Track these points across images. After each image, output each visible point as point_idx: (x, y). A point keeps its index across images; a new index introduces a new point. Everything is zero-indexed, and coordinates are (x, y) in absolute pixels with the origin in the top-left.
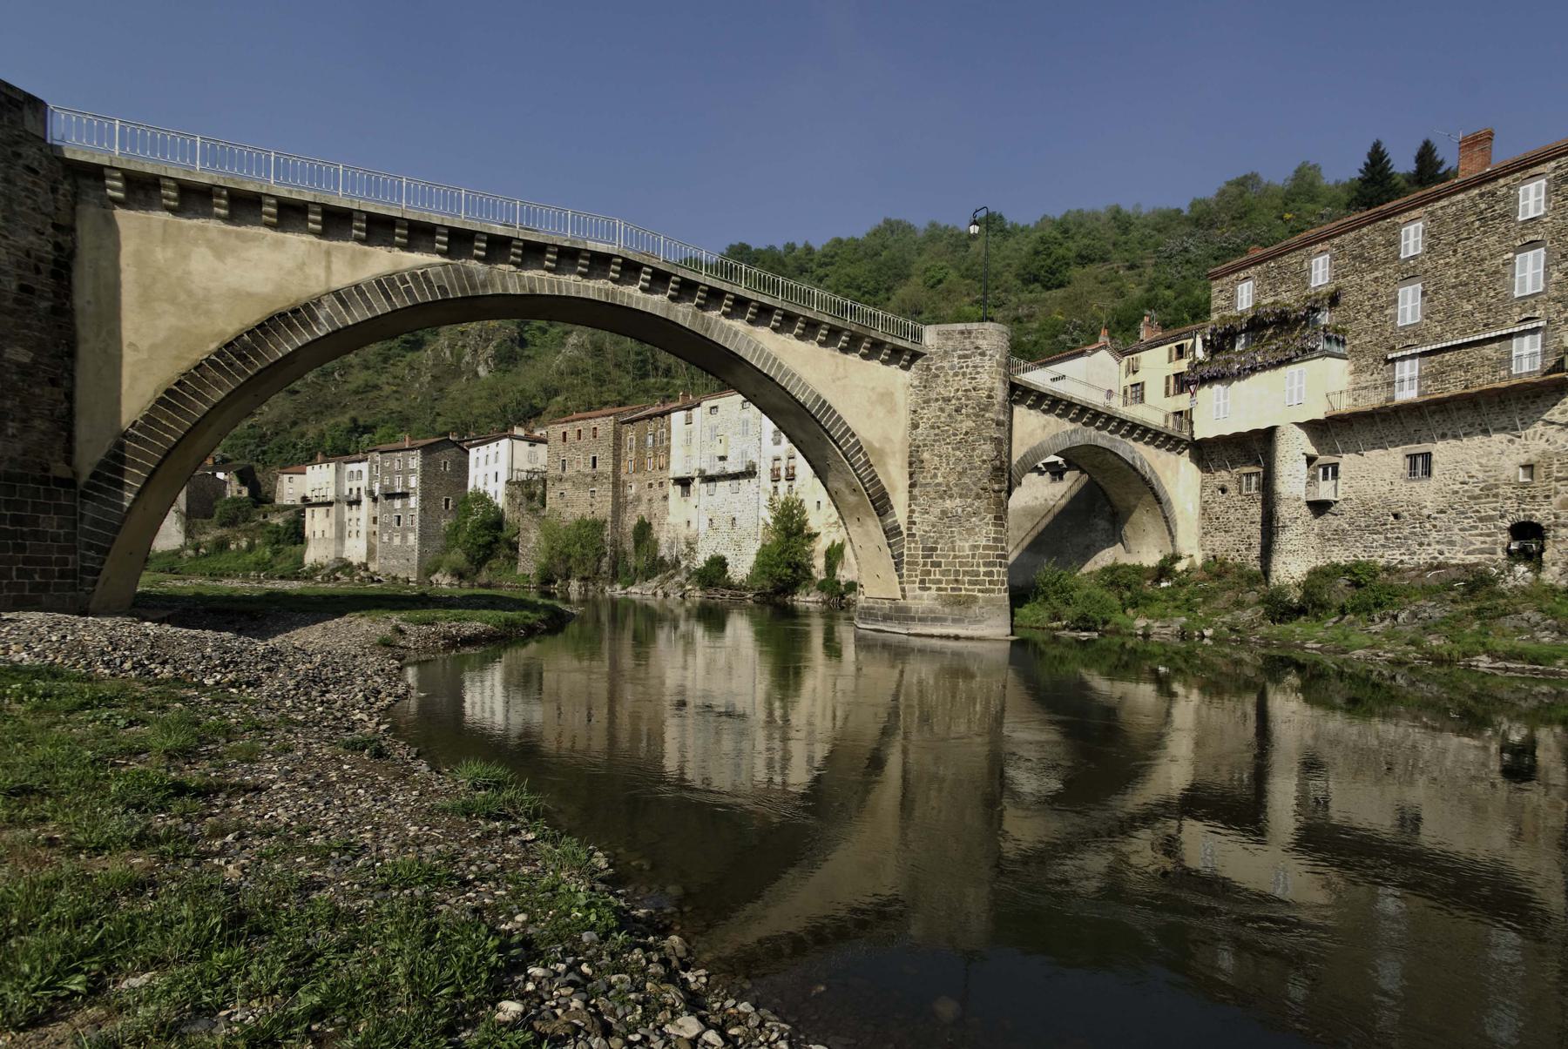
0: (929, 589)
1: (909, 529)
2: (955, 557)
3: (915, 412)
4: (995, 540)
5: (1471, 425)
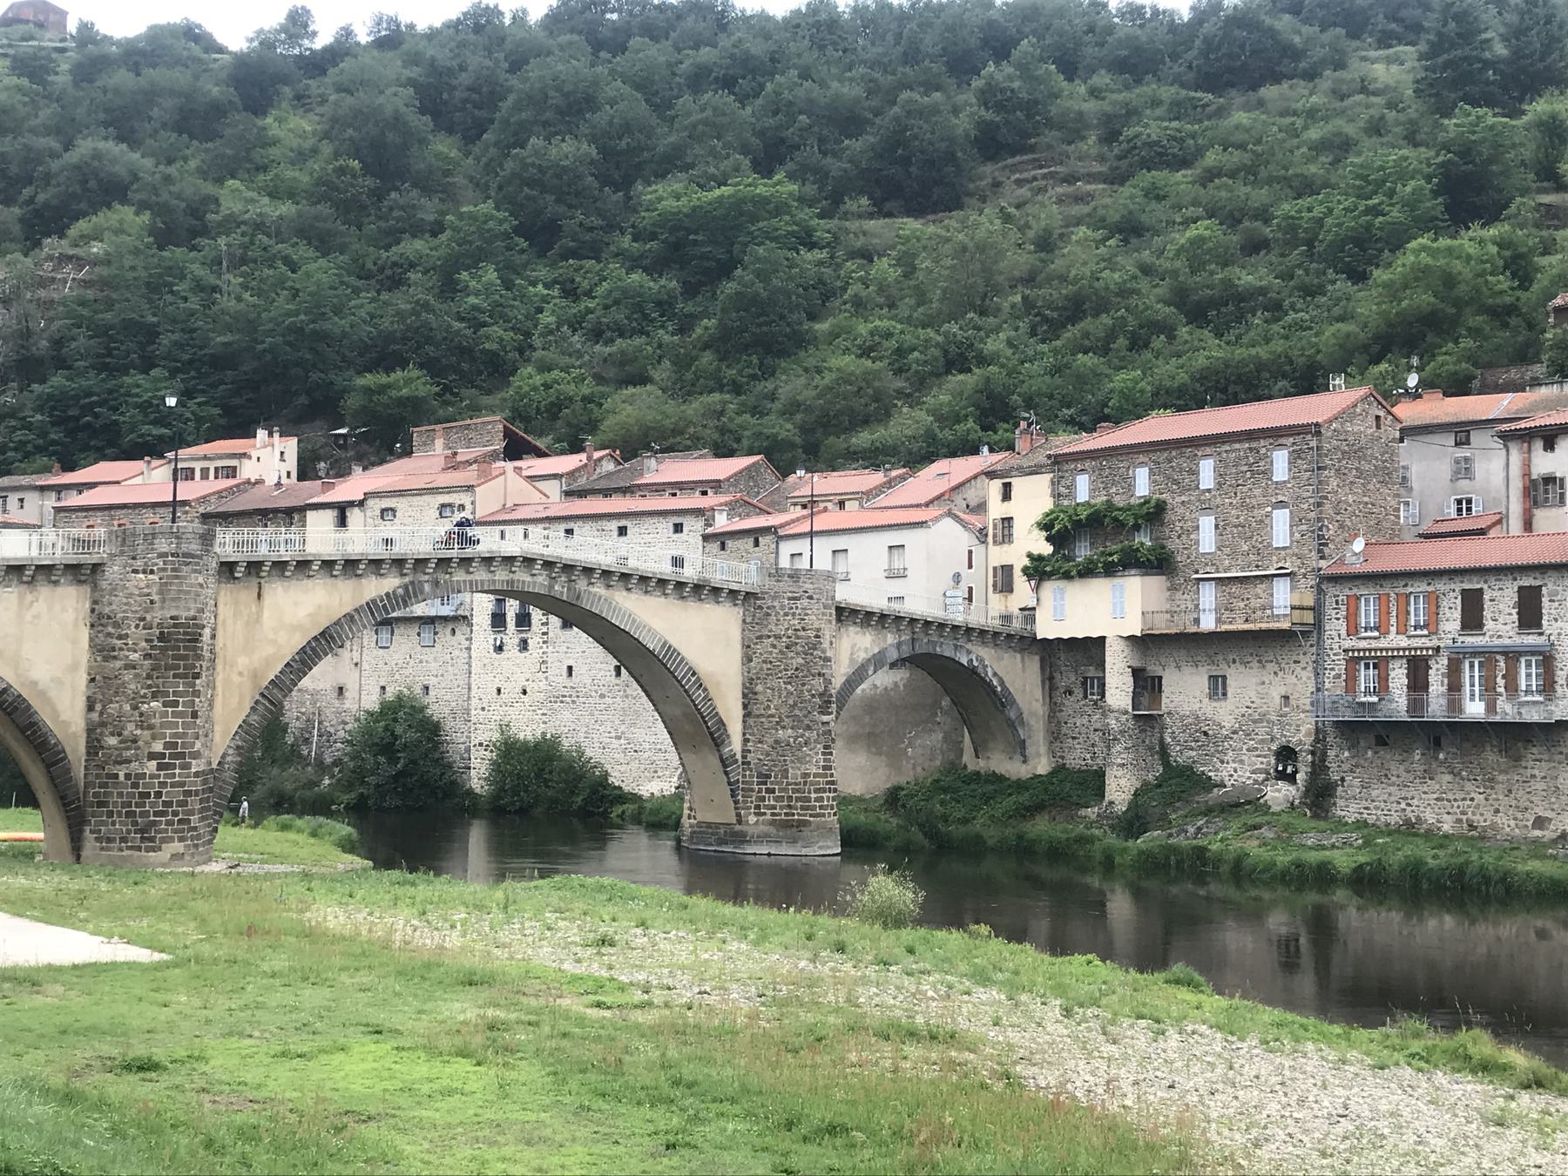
0: (765, 814)
1: (744, 757)
2: (788, 784)
3: (749, 647)
4: (825, 768)
5: (1251, 655)
